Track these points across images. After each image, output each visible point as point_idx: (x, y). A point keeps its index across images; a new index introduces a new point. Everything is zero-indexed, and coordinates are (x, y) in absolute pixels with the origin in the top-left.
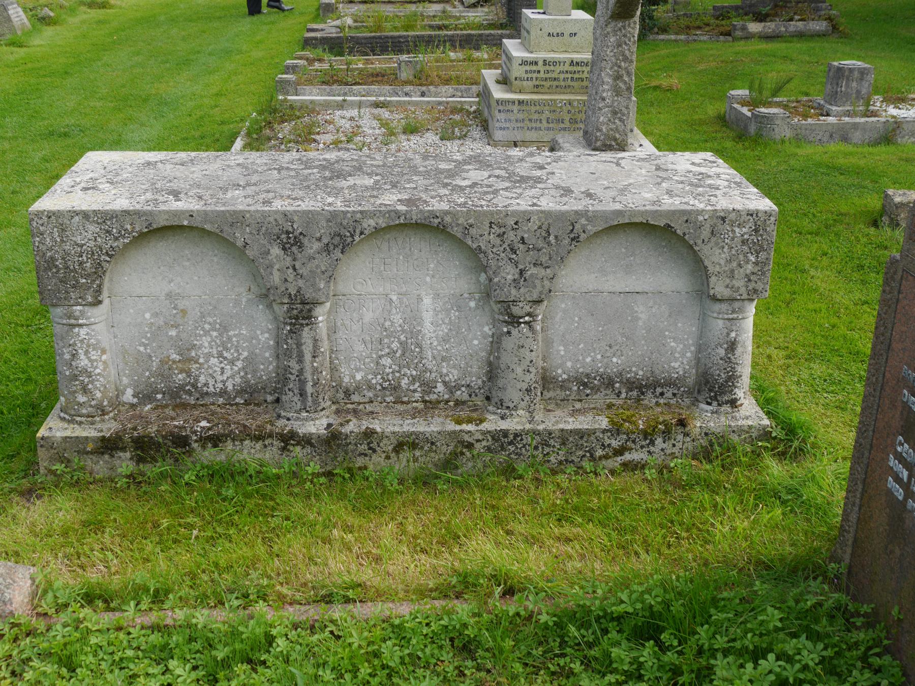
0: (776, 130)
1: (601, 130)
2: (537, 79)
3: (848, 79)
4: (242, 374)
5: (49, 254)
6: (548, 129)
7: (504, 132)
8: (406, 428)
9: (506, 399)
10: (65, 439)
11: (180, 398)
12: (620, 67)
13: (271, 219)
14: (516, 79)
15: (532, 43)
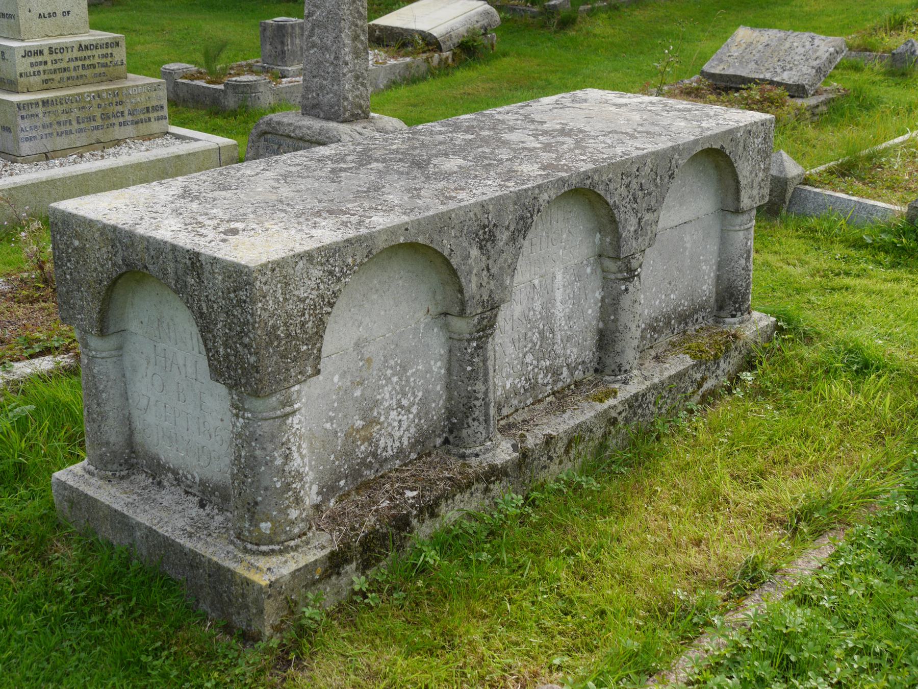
0: (261, 98)
1: (346, 99)
2: (44, 71)
3: (291, 36)
4: (417, 421)
5: (271, 322)
6: (80, 131)
7: (31, 143)
8: (572, 423)
9: (624, 362)
10: (293, 574)
11: (362, 476)
12: (357, 25)
13: (471, 214)
14: (21, 75)
15: (22, 29)
